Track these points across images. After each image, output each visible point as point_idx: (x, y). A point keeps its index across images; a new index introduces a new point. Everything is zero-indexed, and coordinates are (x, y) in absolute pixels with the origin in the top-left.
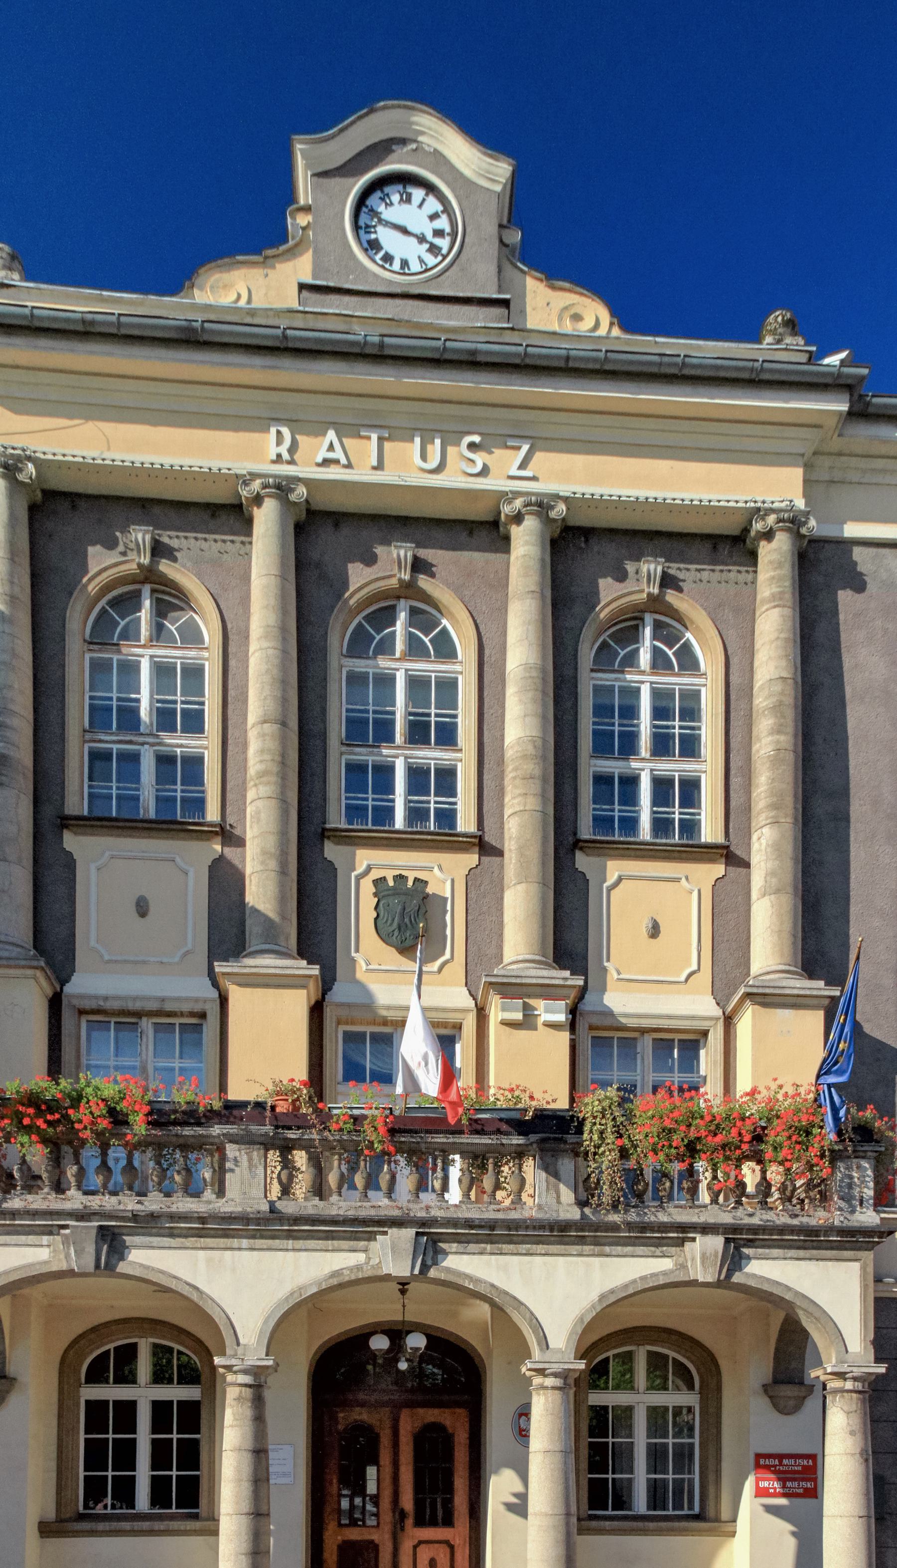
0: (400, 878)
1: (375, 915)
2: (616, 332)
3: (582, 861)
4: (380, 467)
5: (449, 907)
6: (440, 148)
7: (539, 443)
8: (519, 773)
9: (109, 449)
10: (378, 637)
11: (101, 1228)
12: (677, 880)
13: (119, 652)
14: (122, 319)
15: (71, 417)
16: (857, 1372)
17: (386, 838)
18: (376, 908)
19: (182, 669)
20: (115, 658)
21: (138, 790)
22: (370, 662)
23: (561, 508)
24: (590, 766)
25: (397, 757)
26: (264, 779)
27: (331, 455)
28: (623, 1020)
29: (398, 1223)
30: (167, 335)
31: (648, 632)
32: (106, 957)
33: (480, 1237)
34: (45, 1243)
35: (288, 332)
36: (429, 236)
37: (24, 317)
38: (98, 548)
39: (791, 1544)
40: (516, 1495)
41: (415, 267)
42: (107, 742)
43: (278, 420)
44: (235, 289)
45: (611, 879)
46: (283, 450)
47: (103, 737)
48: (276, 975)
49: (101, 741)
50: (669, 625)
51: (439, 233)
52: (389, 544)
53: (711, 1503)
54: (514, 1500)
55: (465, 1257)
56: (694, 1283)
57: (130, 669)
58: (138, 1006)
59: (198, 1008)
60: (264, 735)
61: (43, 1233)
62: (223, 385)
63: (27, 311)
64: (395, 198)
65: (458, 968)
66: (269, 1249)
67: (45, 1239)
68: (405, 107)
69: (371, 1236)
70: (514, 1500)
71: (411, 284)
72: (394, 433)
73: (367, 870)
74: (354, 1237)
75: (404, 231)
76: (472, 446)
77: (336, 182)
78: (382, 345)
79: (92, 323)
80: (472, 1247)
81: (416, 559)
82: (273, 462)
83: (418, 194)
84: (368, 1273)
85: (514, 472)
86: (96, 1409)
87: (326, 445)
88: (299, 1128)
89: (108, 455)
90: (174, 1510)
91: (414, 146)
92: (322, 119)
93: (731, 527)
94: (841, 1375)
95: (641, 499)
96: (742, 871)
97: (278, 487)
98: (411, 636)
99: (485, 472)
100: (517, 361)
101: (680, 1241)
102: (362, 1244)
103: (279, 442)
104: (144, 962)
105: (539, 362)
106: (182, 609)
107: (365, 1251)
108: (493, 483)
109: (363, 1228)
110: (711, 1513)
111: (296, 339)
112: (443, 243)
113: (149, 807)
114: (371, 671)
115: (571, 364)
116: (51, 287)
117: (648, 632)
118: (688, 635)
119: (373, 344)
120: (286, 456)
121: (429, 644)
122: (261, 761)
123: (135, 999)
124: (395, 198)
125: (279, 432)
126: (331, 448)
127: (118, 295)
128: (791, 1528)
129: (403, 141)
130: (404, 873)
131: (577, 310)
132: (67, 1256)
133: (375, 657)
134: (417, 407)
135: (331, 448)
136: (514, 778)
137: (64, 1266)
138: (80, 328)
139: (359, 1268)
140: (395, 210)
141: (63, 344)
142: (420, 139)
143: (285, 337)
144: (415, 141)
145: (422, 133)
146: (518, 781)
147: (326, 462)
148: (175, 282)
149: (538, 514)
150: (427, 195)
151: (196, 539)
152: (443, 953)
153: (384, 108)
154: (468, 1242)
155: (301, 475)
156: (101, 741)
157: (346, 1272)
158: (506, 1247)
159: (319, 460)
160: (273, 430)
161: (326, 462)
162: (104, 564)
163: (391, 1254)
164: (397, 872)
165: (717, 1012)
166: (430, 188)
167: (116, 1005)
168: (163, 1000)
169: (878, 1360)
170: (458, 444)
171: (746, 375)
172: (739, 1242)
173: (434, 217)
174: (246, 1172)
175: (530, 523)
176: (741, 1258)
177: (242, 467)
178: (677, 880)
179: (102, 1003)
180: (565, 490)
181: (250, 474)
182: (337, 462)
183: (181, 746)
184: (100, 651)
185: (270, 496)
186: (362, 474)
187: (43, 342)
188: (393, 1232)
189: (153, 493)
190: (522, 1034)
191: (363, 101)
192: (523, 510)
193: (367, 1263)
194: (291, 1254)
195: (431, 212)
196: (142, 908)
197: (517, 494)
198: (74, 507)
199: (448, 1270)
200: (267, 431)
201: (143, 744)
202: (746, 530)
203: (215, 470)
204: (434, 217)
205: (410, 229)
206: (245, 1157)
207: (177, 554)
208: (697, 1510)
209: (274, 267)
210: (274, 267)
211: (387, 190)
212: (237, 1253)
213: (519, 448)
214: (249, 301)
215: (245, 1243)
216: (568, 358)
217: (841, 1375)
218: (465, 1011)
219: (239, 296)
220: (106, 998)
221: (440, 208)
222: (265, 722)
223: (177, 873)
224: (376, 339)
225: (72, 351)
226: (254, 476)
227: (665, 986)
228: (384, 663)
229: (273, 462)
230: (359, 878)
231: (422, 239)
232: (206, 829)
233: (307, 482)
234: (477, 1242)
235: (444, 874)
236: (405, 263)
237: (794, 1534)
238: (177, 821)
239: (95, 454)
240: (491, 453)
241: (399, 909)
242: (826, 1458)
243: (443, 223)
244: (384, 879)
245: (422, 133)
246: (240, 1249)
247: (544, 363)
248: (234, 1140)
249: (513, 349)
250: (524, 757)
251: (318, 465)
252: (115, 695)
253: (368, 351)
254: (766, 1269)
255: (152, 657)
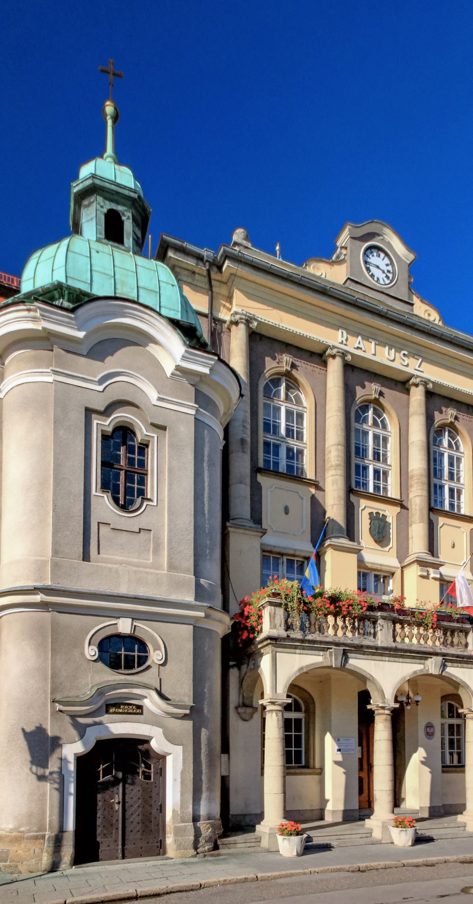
0: (377, 513)
1: (369, 527)
2: (440, 324)
3: (353, 498)
4: (374, 355)
5: (391, 527)
6: (391, 242)
7: (425, 359)
8: (420, 481)
9: (282, 322)
10: (363, 416)
11: (344, 650)
12: (460, 528)
13: (273, 402)
14: (272, 266)
15: (269, 306)
16: (280, 702)
17: (371, 496)
18: (370, 524)
19: (297, 414)
20: (272, 404)
21: (278, 460)
22: (361, 425)
23: (255, 324)
24: (354, 461)
25: (370, 464)
26: (339, 467)
27: (359, 346)
28: (367, 564)
29: (436, 654)
30: (316, 288)
31: (447, 433)
32: (274, 529)
33: (319, 649)
34: (321, 654)
35: (358, 300)
36: (386, 271)
37: (268, 267)
38: (359, 387)
39: (343, 777)
40: (424, 758)
41: (382, 282)
42: (270, 438)
43: (345, 329)
44: (319, 270)
45: (440, 525)
46: (344, 339)
47: (268, 436)
48: (348, 548)
49: (268, 438)
50: (453, 433)
51: (389, 271)
52: (372, 383)
53: (311, 761)
54: (423, 760)
55: (453, 668)
56: (431, 675)
57: (277, 409)
58: (283, 551)
59: (307, 555)
60: (338, 450)
61: (321, 651)
62: (348, 318)
63: (269, 266)
64: (375, 254)
65: (394, 551)
66: (394, 662)
67: (321, 653)
68: (382, 224)
69: (426, 659)
70: (423, 760)
71: (381, 288)
72: (382, 343)
73: (365, 508)
74: (421, 658)
75: (378, 267)
76: (404, 355)
77: (357, 242)
78: (387, 313)
79: (291, 276)
80: (455, 665)
81: (292, 363)
82: (340, 343)
83: (382, 255)
84: (425, 673)
85: (417, 368)
86: (451, 726)
87: (358, 342)
88: (403, 615)
89: (281, 325)
90: (293, 765)
91: (382, 238)
92: (357, 220)
93: (317, 349)
94: (273, 703)
95: (305, 336)
96: (406, 511)
97: (247, 320)
98: (374, 418)
99: (407, 366)
100: (266, 269)
101: (326, 649)
102: (423, 661)
103: (342, 336)
104: (288, 533)
105: (274, 272)
106: (294, 389)
107: (424, 664)
108: (410, 370)
109: (423, 655)
110: (311, 765)
111: (359, 302)
112: (390, 276)
113: (283, 468)
114: (361, 429)
115: (443, 337)
116: (265, 254)
117: (447, 433)
118: (385, 415)
119: (384, 312)
120: (344, 342)
121: (379, 423)
122: (338, 460)
123: (285, 548)
124: (375, 254)
125: (342, 332)
126: (359, 343)
127: (288, 263)
128: (344, 770)
129: (379, 235)
130: (379, 512)
131: (429, 312)
132: (331, 660)
133: (362, 424)
134: (388, 336)
135: (359, 343)
136: (418, 482)
137: (329, 664)
138: (286, 277)
139: (421, 670)
140: (374, 259)
141: (277, 280)
142: (384, 236)
143: (356, 301)
144: (382, 236)
145: (386, 235)
146: (419, 484)
147: (358, 348)
148: (300, 262)
149: (245, 324)
150: (385, 256)
151: (304, 363)
152: (389, 544)
153: (376, 222)
154: (454, 663)
155: (350, 351)
156: (268, 438)
157: (418, 672)
158: (465, 665)
159: (356, 347)
160: (340, 331)
161: (358, 348)
162: (271, 366)
163: (432, 666)
164: (377, 511)
165: (398, 565)
166: (387, 254)
167: (277, 550)
168: (295, 550)
169: (288, 696)
170: (400, 352)
171: (449, 339)
172: (348, 650)
173: (387, 265)
174: (387, 631)
175: (421, 388)
176: (348, 658)
177: (331, 343)
178: (460, 528)
179: (272, 548)
180: (433, 379)
181: (333, 346)
182: (361, 349)
183: (296, 445)
184: (267, 400)
185: (339, 356)
186: (368, 355)
187: (269, 277)
188: (434, 657)
189: (291, 342)
190: (425, 580)
191: (371, 218)
192: (239, 321)
193: (424, 669)
194: (401, 664)
195: (387, 263)
196: (287, 511)
197: (418, 376)
198: (353, 371)
199: (448, 673)
200: (338, 330)
201: (283, 442)
202: (408, 381)
203: (321, 341)
204: (387, 265)
205: (380, 267)
206: (386, 625)
207: (298, 368)
208: (303, 763)
209: (333, 266)
210: (333, 266)
211: (373, 250)
212: (384, 662)
213: (418, 359)
214: (325, 277)
215: (387, 659)
216: (442, 335)
217: (383, 708)
218: (398, 568)
219: (322, 274)
220: (275, 547)
221: (389, 262)
222: (339, 445)
223: (298, 497)
224: (386, 311)
225: (279, 283)
226: (334, 347)
227: (457, 566)
228: (365, 426)
229: (340, 343)
230: (362, 510)
231: (384, 272)
232: (312, 482)
233: (352, 355)
234: (457, 663)
235: (391, 513)
236: (378, 279)
237: (344, 773)
238: (294, 475)
239: (277, 323)
240: (409, 359)
241: (378, 525)
242: (466, 743)
243: (390, 268)
244: (372, 513)
245: (386, 235)
246: (385, 661)
247: (361, 306)
248: (384, 618)
249: (250, 258)
250: (422, 475)
251: (355, 348)
252: (272, 419)
253: (381, 314)
254: (356, 662)
255: (286, 407)
